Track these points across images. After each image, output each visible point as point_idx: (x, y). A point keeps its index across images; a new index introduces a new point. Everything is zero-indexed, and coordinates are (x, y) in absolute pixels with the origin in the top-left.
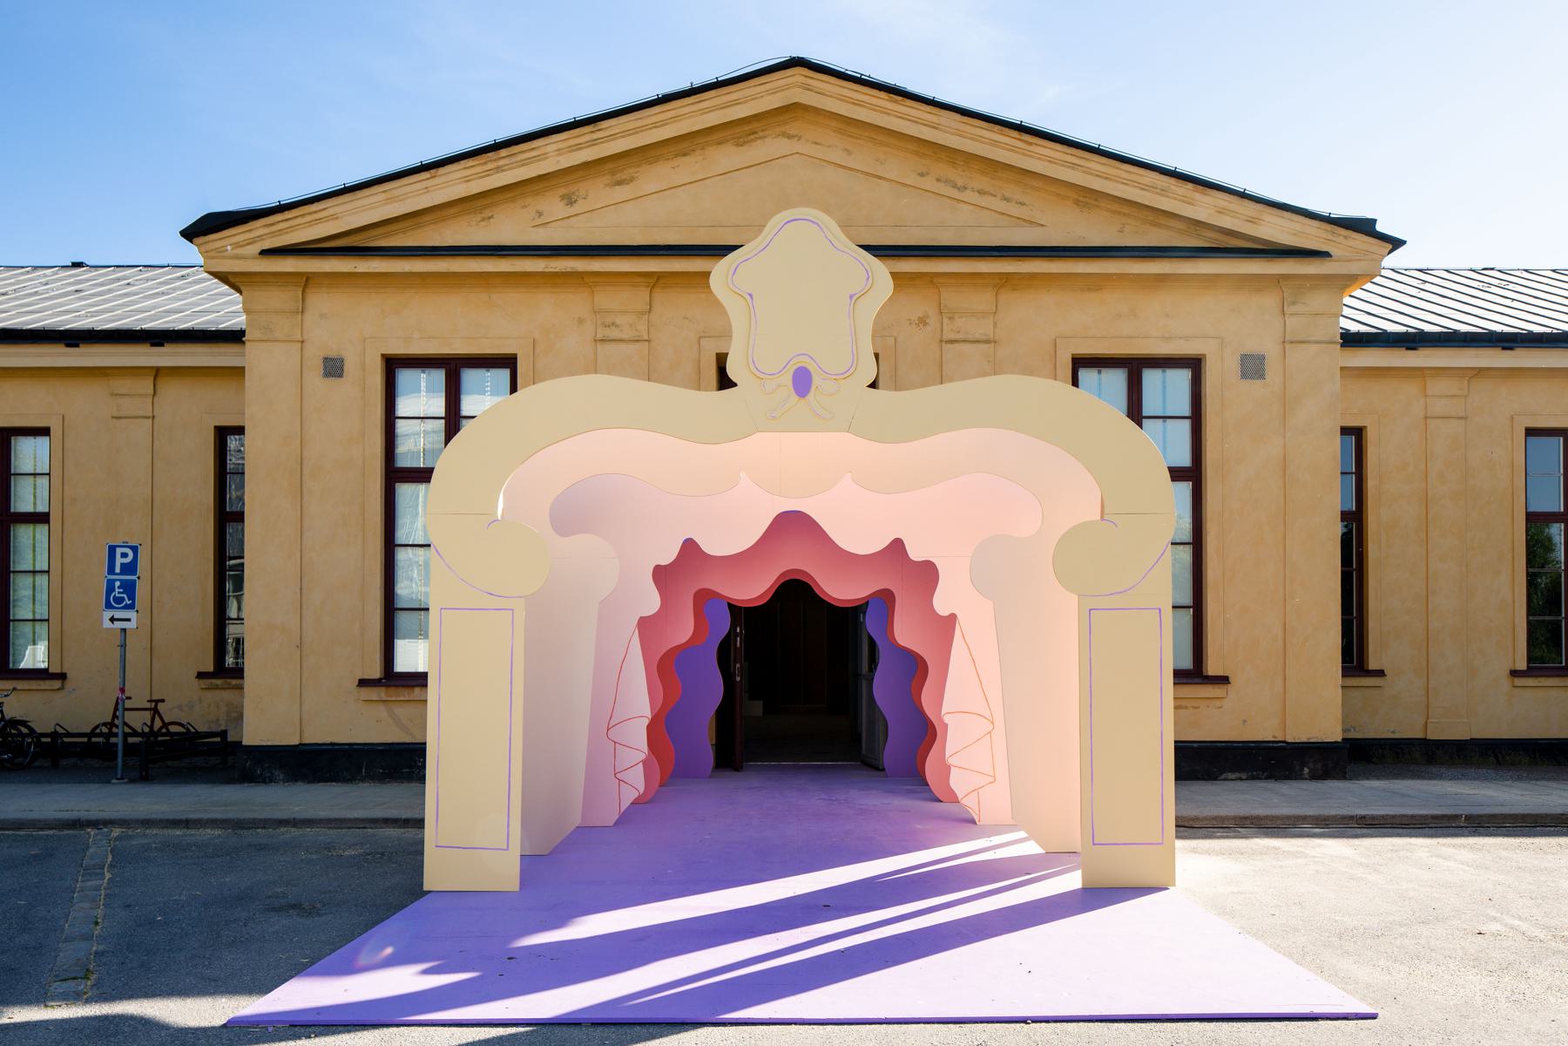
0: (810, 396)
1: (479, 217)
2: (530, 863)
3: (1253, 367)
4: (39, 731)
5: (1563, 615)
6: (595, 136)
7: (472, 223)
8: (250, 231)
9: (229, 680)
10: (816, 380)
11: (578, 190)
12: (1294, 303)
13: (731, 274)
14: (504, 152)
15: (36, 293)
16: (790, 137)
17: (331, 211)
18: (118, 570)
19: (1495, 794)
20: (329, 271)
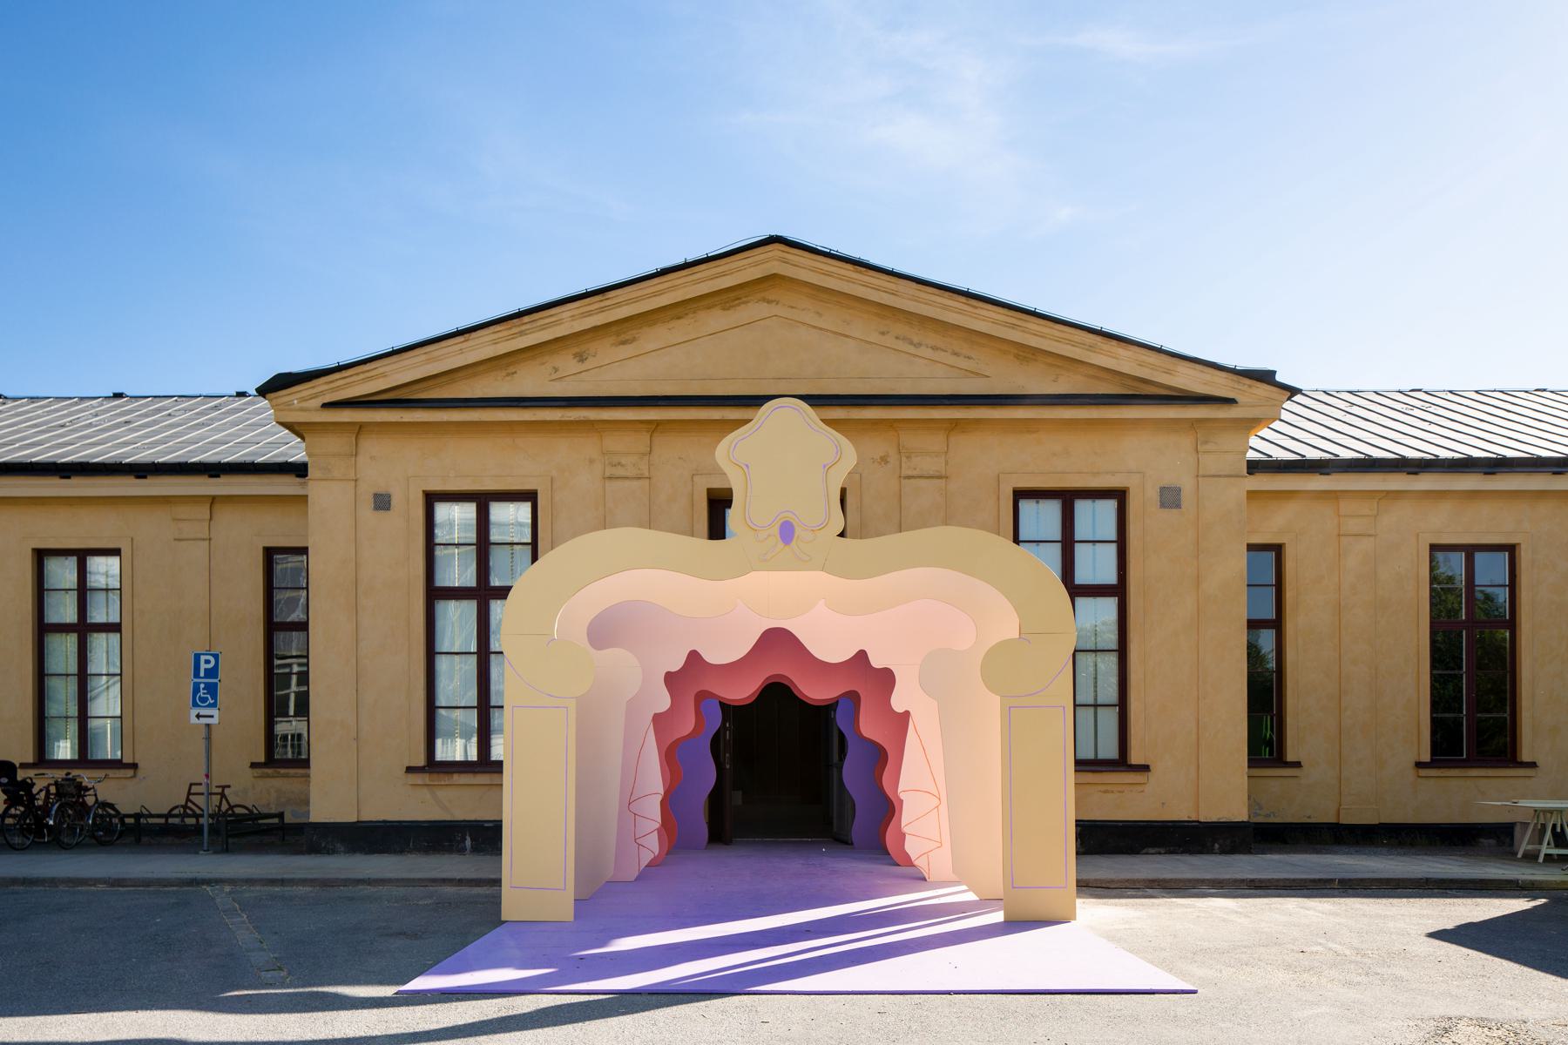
0: (794, 543)
1: (504, 373)
2: (581, 904)
3: (1170, 498)
4: (123, 812)
5: (1464, 713)
6: (603, 304)
7: (499, 378)
8: (313, 387)
9: (279, 770)
10: (798, 531)
11: (588, 349)
12: (1206, 442)
13: (732, 449)
14: (526, 319)
15: (90, 425)
16: (769, 302)
17: (381, 370)
18: (202, 674)
19: (1373, 864)
20: (379, 420)
